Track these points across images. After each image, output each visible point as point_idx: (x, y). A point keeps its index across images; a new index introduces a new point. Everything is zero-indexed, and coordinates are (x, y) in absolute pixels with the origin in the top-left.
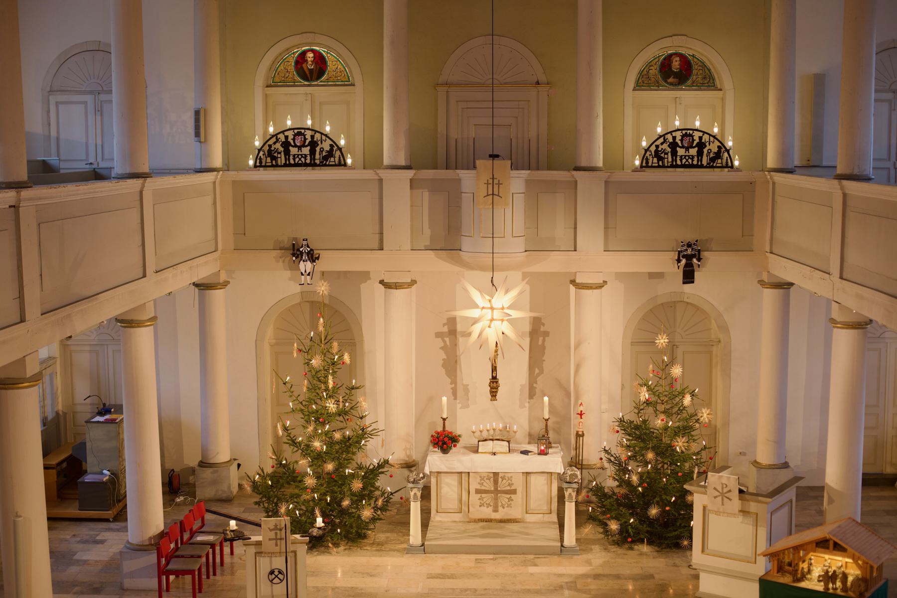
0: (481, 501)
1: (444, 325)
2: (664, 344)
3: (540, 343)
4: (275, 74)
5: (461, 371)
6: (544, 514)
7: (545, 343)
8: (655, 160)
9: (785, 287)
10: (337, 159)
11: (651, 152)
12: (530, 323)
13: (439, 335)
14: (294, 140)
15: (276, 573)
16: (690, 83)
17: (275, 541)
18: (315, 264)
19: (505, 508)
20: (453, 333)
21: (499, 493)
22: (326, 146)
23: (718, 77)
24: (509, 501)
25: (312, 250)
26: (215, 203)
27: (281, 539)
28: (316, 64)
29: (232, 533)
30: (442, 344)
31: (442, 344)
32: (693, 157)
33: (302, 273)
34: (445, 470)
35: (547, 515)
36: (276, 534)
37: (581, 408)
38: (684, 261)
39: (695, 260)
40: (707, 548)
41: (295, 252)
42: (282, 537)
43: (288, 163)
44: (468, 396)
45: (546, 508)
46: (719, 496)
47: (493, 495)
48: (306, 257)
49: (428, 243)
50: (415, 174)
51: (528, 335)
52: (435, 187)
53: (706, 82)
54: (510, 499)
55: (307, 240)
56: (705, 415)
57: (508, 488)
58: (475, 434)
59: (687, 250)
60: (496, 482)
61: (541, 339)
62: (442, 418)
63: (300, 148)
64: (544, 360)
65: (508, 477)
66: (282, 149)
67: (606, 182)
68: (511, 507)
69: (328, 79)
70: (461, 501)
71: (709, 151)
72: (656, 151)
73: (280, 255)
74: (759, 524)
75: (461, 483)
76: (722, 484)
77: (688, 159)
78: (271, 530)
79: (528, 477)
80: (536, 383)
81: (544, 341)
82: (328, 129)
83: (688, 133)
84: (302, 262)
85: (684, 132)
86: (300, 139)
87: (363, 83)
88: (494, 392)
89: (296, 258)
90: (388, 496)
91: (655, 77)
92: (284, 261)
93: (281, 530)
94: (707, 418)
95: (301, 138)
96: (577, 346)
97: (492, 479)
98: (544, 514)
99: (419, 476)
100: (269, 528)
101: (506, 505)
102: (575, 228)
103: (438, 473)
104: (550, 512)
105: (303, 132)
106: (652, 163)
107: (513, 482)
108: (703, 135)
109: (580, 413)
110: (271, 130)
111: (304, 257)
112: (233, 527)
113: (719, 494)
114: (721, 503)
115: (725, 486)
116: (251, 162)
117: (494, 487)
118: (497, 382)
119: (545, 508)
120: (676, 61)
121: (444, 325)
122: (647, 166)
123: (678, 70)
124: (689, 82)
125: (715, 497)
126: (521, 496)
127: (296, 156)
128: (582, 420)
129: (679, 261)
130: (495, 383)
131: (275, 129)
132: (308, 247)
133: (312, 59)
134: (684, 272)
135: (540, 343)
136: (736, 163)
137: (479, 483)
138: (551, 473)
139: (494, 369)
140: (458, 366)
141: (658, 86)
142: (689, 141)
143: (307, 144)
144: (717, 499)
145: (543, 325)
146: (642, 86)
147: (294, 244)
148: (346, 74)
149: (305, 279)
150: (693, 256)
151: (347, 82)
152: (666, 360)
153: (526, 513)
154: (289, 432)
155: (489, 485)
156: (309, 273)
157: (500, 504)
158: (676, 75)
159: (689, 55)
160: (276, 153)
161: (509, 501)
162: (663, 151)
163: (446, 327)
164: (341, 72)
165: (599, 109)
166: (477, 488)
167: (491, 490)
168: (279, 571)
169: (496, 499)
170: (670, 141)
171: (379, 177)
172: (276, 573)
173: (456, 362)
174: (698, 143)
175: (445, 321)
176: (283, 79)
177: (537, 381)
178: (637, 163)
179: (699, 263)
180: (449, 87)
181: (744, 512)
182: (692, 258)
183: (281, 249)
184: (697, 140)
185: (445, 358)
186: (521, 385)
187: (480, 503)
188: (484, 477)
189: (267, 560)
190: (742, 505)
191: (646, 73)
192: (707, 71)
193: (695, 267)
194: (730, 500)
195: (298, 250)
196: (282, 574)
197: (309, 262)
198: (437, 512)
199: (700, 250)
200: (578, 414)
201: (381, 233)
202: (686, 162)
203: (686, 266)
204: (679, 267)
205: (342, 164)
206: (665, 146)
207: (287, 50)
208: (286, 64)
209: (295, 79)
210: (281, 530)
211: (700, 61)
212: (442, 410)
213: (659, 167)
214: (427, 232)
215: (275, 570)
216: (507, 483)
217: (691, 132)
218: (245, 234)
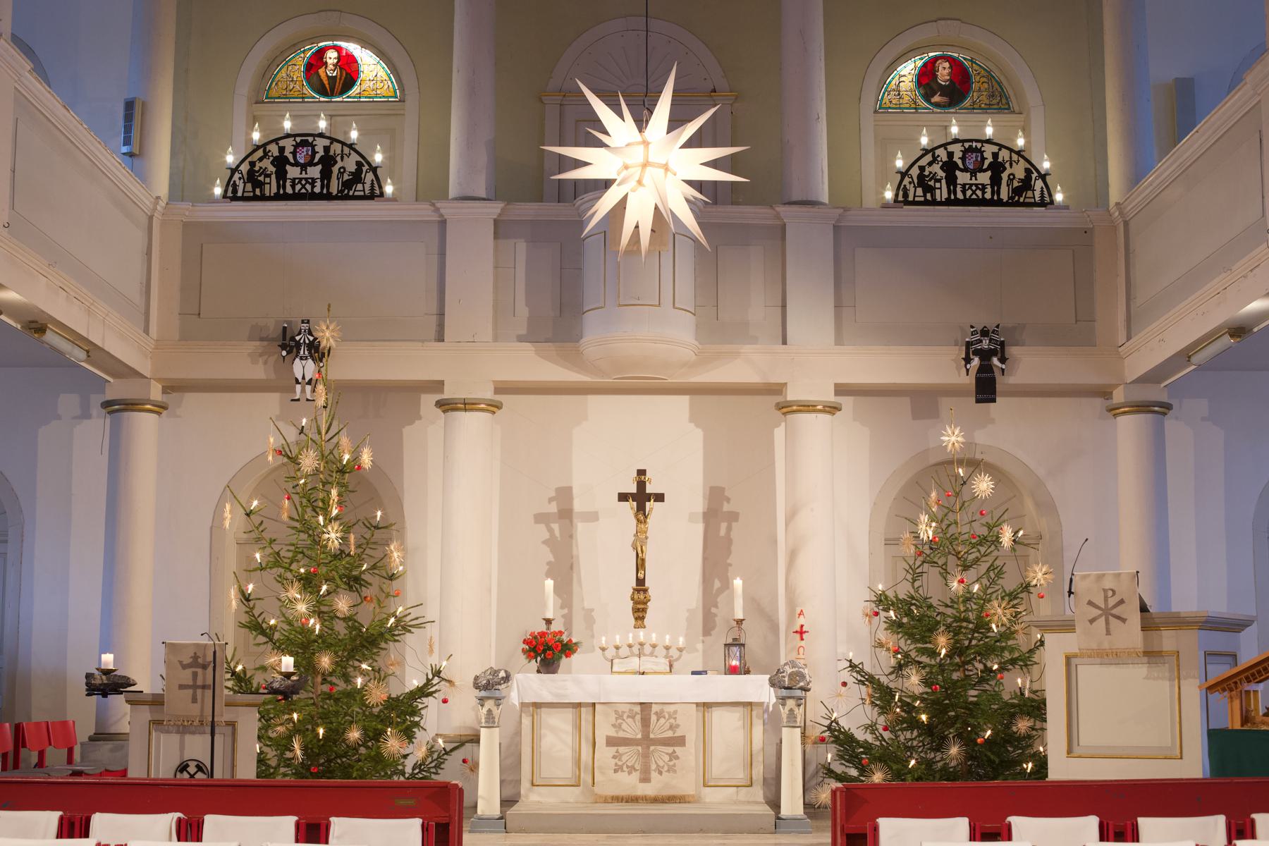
0: (617, 760)
1: (550, 500)
2: (956, 444)
3: (723, 532)
4: (272, 83)
5: (577, 546)
6: (738, 786)
7: (732, 533)
8: (920, 191)
9: (1156, 409)
10: (367, 187)
11: (912, 177)
12: (704, 497)
13: (540, 518)
14: (294, 153)
15: (192, 769)
16: (968, 104)
17: (190, 691)
18: (321, 365)
19: (664, 774)
20: (566, 514)
21: (653, 745)
22: (350, 164)
23: (1015, 94)
24: (671, 760)
25: (316, 339)
26: (149, 253)
27: (204, 687)
28: (340, 69)
29: (104, 677)
30: (547, 535)
31: (547, 535)
32: (984, 187)
33: (297, 380)
34: (549, 698)
35: (744, 789)
36: (195, 675)
37: (801, 621)
38: (976, 361)
39: (995, 361)
40: (1078, 745)
41: (287, 342)
42: (207, 683)
43: (281, 192)
44: (592, 630)
45: (741, 776)
46: (1100, 616)
47: (640, 748)
48: (306, 352)
49: (523, 331)
50: (502, 209)
51: (701, 520)
52: (537, 233)
53: (994, 102)
54: (673, 756)
55: (308, 322)
56: (1040, 575)
57: (670, 734)
58: (606, 652)
59: (981, 341)
60: (646, 723)
61: (724, 526)
62: (544, 619)
63: (304, 167)
64: (730, 565)
65: (669, 713)
66: (274, 170)
67: (837, 228)
68: (675, 771)
69: (360, 93)
70: (578, 762)
71: (1011, 178)
72: (921, 177)
73: (260, 351)
74: (1183, 673)
75: (578, 727)
76: (1105, 591)
77: (976, 190)
78: (184, 667)
79: (706, 714)
80: (716, 606)
81: (729, 529)
82: (354, 135)
83: (974, 147)
84: (297, 360)
85: (967, 145)
86: (305, 153)
87: (419, 92)
88: (640, 612)
89: (288, 353)
90: (439, 757)
91: (909, 93)
92: (265, 363)
93: (204, 667)
94: (1045, 579)
95: (307, 151)
96: (791, 516)
97: (638, 717)
98: (738, 786)
99: (498, 675)
100: (181, 662)
101: (666, 768)
102: (784, 306)
103: (537, 706)
104: (749, 783)
105: (310, 141)
106: (915, 196)
107: (678, 722)
108: (1000, 150)
109: (799, 629)
110: (256, 136)
111: (302, 352)
112: (107, 664)
113: (1100, 612)
114: (1105, 632)
115: (1110, 593)
116: (218, 191)
117: (643, 732)
118: (645, 591)
119: (740, 775)
120: (944, 68)
121: (550, 500)
122: (907, 202)
123: (947, 83)
124: (967, 102)
125: (1092, 621)
126: (693, 751)
127: (297, 181)
128: (803, 643)
129: (968, 360)
130: (642, 593)
131: (262, 136)
132: (310, 333)
133: (336, 61)
134: (978, 380)
135: (723, 532)
136: (1059, 197)
137: (614, 726)
138: (750, 704)
139: (640, 564)
140: (575, 576)
141: (915, 108)
142: (977, 160)
143: (316, 160)
144: (1094, 624)
145: (728, 500)
146: (890, 108)
147: (285, 328)
148: (391, 86)
149: (303, 391)
150: (992, 353)
151: (391, 97)
152: (962, 475)
153: (705, 785)
154: (251, 603)
155: (632, 729)
156: (311, 380)
157: (653, 766)
158: (944, 91)
159: (965, 59)
160: (263, 176)
161: (671, 760)
162: (933, 176)
163: (554, 504)
164: (382, 82)
165: (821, 108)
166: (609, 735)
167: (636, 740)
168: (197, 766)
169: (646, 756)
170: (944, 160)
171: (441, 216)
172: (192, 769)
173: (571, 568)
174: (991, 163)
175: (553, 494)
176: (284, 93)
177: (717, 602)
178: (889, 195)
179: (1004, 367)
180: (564, 96)
181: (1152, 655)
182: (991, 356)
183: (262, 339)
184: (989, 159)
185: (553, 560)
186: (688, 610)
187: (616, 764)
188: (624, 712)
189: (175, 738)
190: (1145, 639)
191: (894, 87)
192: (996, 86)
193: (997, 374)
194: (1124, 620)
195: (293, 339)
196: (204, 773)
197: (310, 361)
198: (533, 785)
199: (1003, 341)
200: (796, 632)
201: (441, 315)
202: (972, 195)
203: (981, 369)
204: (968, 370)
205: (375, 194)
206: (936, 168)
207: (294, 45)
208: (290, 68)
209: (305, 92)
210: (204, 667)
211: (985, 69)
212: (544, 605)
213: (926, 203)
214: (523, 311)
215: (189, 763)
216: (668, 725)
217: (979, 145)
218: (199, 314)
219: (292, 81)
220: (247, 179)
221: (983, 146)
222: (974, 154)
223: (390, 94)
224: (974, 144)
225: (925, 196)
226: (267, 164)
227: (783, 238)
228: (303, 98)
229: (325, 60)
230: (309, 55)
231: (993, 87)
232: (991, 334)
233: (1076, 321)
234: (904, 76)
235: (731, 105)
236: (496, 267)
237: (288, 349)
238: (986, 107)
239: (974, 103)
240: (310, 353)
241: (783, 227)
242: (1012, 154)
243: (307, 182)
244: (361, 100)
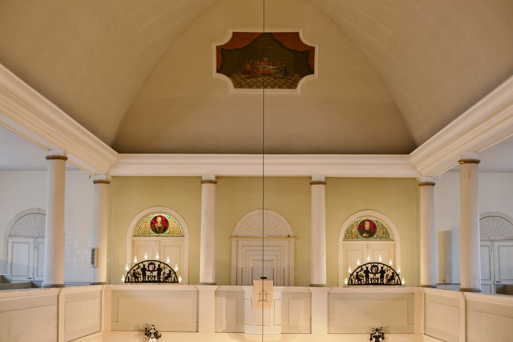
8: (356, 281)
23: (391, 233)
32: (378, 279)
38: (374, 339)
39: (380, 339)
41: (147, 332)
48: (153, 336)
53: (384, 236)
59: (376, 333)
67: (328, 293)
69: (169, 233)
71: (387, 276)
72: (357, 275)
77: (375, 280)
83: (375, 265)
84: (150, 338)
85: (373, 264)
91: (355, 233)
92: (140, 338)
106: (355, 282)
108: (384, 266)
111: (152, 336)
116: (123, 280)
124: (375, 236)
129: (371, 339)
133: (161, 221)
142: (376, 270)
148: (179, 230)
150: (380, 336)
151: (180, 234)
158: (367, 232)
159: (374, 221)
170: (365, 270)
171: (197, 289)
174: (381, 270)
176: (143, 232)
179: (383, 341)
183: (139, 331)
192: (385, 230)
195: (149, 331)
197: (155, 339)
199: (383, 333)
201: (198, 322)
206: (362, 273)
208: (145, 223)
209: (150, 232)
211: (381, 224)
213: (359, 284)
217: (377, 264)
218: (118, 321)
219: (146, 228)
220: (133, 275)
221: (378, 265)
222: (375, 268)
223: (179, 233)
224: (375, 264)
225: (358, 282)
226: (139, 270)
227: (311, 297)
228: (150, 234)
229: (157, 221)
230: (151, 219)
231: (384, 231)
232: (379, 330)
233: (408, 325)
234: (354, 227)
235: (294, 241)
236: (216, 306)
237: (147, 335)
238: (381, 238)
239: (377, 236)
240: (155, 336)
241: (311, 293)
242: (388, 267)
243: (153, 277)
244: (170, 235)
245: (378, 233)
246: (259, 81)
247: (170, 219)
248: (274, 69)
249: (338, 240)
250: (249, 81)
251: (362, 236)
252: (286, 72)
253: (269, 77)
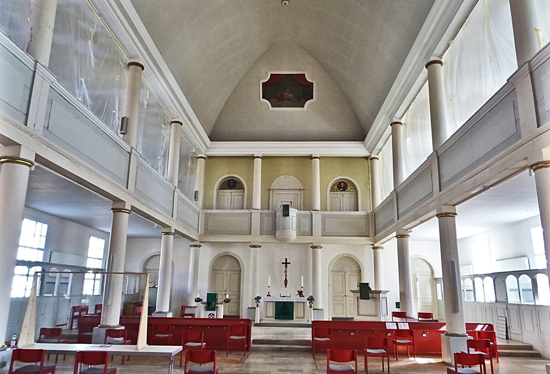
158: (342, 188)
245: (348, 189)
246: (284, 103)
247: (290, 185)
248: (292, 96)
249: (451, 206)
250: (279, 103)
251: (339, 190)
252: (298, 98)
253: (289, 101)
